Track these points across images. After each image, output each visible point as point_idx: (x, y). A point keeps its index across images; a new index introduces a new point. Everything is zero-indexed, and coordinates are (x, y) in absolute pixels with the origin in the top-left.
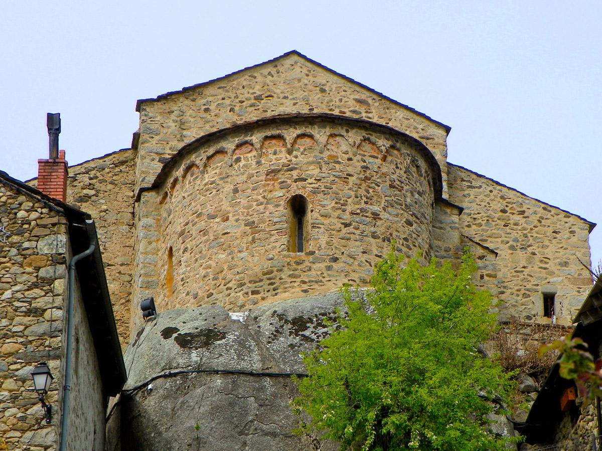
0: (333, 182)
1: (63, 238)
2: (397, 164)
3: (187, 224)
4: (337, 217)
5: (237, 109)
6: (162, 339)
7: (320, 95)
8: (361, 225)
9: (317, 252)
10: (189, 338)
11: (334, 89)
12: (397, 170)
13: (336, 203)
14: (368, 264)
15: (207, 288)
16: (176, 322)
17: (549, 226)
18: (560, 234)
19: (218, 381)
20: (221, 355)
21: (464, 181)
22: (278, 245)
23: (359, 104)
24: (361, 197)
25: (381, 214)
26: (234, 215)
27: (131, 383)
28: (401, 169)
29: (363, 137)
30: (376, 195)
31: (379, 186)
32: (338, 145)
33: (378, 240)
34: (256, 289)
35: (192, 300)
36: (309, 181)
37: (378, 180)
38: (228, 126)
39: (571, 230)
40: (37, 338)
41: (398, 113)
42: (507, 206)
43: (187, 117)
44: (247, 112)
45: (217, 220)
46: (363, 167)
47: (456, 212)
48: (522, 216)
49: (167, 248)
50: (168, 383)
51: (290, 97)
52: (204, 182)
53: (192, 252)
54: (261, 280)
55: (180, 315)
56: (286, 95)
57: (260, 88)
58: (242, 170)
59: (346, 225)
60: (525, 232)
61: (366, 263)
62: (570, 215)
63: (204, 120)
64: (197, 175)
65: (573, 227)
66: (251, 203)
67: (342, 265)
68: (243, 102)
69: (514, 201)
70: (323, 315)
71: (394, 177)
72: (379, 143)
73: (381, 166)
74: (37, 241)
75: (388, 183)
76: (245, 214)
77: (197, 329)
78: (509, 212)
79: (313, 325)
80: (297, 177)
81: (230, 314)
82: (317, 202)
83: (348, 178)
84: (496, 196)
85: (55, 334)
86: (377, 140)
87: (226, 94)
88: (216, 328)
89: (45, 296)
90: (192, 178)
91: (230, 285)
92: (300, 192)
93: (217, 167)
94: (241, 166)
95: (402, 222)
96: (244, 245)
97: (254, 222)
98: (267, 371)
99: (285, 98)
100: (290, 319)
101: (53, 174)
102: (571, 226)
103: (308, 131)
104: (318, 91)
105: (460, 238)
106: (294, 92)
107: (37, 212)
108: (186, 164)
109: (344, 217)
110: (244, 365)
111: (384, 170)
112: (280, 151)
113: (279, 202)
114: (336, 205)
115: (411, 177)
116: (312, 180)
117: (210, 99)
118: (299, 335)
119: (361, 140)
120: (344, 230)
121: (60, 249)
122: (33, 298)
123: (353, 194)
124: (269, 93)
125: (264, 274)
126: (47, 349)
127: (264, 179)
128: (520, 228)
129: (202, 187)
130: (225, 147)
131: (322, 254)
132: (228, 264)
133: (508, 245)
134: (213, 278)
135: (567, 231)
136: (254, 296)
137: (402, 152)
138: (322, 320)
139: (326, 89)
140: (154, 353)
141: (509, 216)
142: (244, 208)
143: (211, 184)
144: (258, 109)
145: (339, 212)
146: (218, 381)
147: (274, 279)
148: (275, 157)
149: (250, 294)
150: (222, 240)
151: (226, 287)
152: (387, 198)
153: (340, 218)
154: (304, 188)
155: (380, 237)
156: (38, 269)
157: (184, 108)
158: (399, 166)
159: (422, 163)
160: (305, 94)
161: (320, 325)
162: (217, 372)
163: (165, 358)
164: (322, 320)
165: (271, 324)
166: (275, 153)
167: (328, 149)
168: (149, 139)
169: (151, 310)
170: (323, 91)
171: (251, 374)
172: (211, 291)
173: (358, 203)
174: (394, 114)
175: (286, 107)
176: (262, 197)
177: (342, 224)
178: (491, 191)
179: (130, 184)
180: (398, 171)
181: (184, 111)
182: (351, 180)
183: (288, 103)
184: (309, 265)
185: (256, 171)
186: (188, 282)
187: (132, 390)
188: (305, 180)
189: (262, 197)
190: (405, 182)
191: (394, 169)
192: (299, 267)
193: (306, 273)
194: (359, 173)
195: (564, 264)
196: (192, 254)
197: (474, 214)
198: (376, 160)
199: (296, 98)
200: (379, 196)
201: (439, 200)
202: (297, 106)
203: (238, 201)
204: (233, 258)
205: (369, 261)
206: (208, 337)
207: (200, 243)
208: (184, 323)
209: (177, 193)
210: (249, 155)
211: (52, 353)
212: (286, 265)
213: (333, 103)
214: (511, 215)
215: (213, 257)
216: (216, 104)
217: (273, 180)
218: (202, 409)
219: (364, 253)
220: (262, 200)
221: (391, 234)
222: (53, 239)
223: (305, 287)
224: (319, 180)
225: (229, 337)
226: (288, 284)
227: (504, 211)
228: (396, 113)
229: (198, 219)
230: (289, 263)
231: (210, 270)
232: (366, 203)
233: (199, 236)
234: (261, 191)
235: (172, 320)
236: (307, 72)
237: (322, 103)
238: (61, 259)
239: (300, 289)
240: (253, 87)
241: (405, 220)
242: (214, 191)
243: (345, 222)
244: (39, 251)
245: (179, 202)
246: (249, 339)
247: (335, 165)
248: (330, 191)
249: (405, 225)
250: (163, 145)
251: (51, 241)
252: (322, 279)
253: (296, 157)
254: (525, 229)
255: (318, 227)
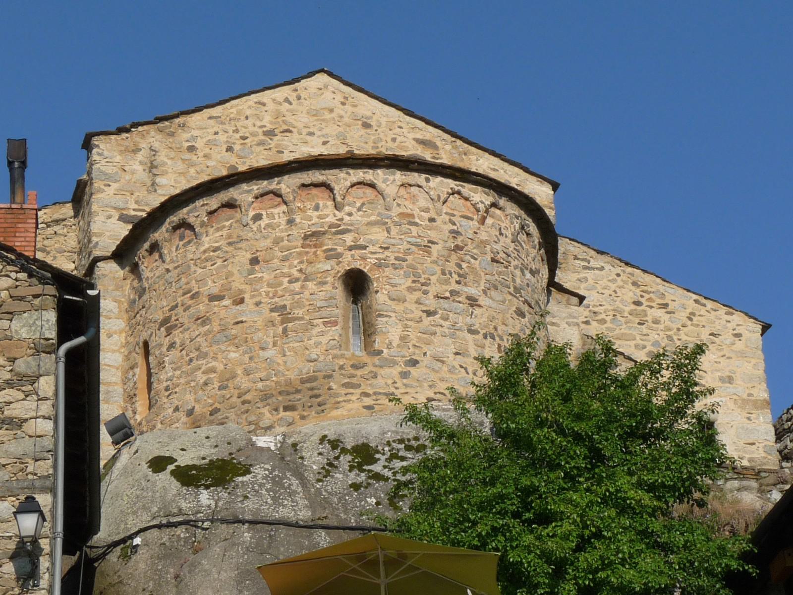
0: (407, 252)
1: (51, 316)
2: (500, 229)
3: (172, 309)
4: (416, 302)
5: (237, 147)
6: (151, 473)
7: (363, 131)
8: (451, 315)
9: (385, 351)
10: (194, 472)
11: (384, 124)
12: (500, 237)
13: (414, 282)
14: (463, 370)
15: (210, 401)
16: (171, 448)
17: (704, 326)
18: (720, 337)
19: (246, 534)
20: (246, 497)
21: (578, 259)
22: (324, 340)
23: (422, 146)
24: (450, 274)
25: (480, 299)
26: (253, 297)
27: (104, 535)
28: (506, 237)
29: (451, 189)
30: (472, 272)
31: (476, 259)
32: (414, 199)
33: (477, 337)
34: (290, 403)
35: (184, 419)
36: (371, 248)
37: (475, 251)
38: (224, 173)
39: (735, 332)
40: (15, 460)
41: (481, 161)
42: (642, 296)
43: (162, 157)
44: (252, 152)
45: (226, 302)
46: (452, 232)
47: (575, 300)
48: (664, 310)
49: (137, 344)
50: (165, 536)
51: (318, 133)
52: (202, 249)
53: (183, 349)
54: (298, 391)
55: (175, 439)
56: (311, 130)
57: (272, 119)
58: (263, 231)
59: (429, 313)
60: (669, 333)
61: (460, 369)
62: (734, 312)
63: (187, 162)
64: (189, 239)
65: (738, 328)
66: (281, 279)
67: (424, 370)
68: (247, 138)
69: (652, 290)
70: (401, 441)
71: (497, 247)
72: (474, 199)
73: (478, 231)
74: (11, 320)
75: (489, 257)
76: (271, 295)
77: (204, 458)
78: (645, 305)
79: (386, 457)
80: (353, 244)
81: (254, 438)
82: (385, 279)
83: (430, 247)
84: (625, 282)
85: (41, 456)
86: (472, 194)
87: (220, 126)
88: (233, 458)
89: (23, 400)
90: (181, 243)
91: (248, 397)
92: (358, 265)
93: (224, 227)
94: (263, 226)
95: (511, 311)
96: (270, 340)
97: (284, 307)
98: (320, 522)
99: (311, 134)
100: (349, 447)
101: (20, 225)
102: (735, 327)
103: (368, 179)
104: (360, 126)
105: (582, 338)
106: (323, 126)
107: (9, 277)
108: (173, 222)
109: (427, 302)
110: (284, 512)
111: (483, 236)
112: (326, 206)
113: (326, 278)
114: (414, 285)
115: (519, 248)
116: (375, 248)
117: (195, 133)
118: (365, 470)
119: (448, 193)
120: (427, 321)
121: (47, 332)
122: (5, 402)
123: (438, 269)
124: (285, 127)
125: (303, 382)
126: (30, 477)
127: (300, 245)
128: (661, 327)
129: (198, 255)
130: (237, 198)
131: (394, 354)
132: (244, 366)
133: (644, 350)
134: (219, 387)
135: (730, 334)
136: (288, 413)
137: (507, 213)
138: (398, 450)
139: (372, 123)
140: (138, 492)
141: (645, 311)
142: (269, 285)
143: (214, 251)
144: (270, 149)
145: (417, 295)
146: (246, 534)
147: (319, 389)
148: (316, 213)
149: (281, 409)
150: (234, 332)
151: (242, 399)
152: (488, 277)
153: (420, 304)
154: (363, 258)
155: (479, 333)
156: (13, 360)
157: (156, 145)
158: (503, 231)
159: (533, 228)
160: (341, 129)
161: (394, 456)
162: (243, 522)
163: (158, 500)
164: (398, 450)
165: (320, 454)
166: (317, 208)
167: (399, 205)
168: (102, 187)
169: (127, 429)
170: (367, 126)
171: (296, 525)
172: (217, 405)
173: (447, 282)
174: (475, 162)
175: (312, 147)
176: (297, 270)
177: (423, 311)
178: (618, 275)
179: (69, 252)
180: (502, 239)
181: (157, 150)
182: (435, 249)
183: (316, 141)
184: (374, 369)
185: (287, 234)
186: (176, 393)
187: (104, 547)
188: (365, 247)
189: (297, 270)
190: (512, 255)
191: (496, 236)
192: (359, 373)
193: (369, 382)
194: (446, 239)
195: (727, 379)
196: (184, 352)
197: (594, 306)
198: (471, 223)
199: (327, 134)
200: (476, 274)
201: (553, 285)
202: (328, 145)
203: (259, 275)
204: (251, 358)
205: (464, 366)
206: (220, 472)
207: (197, 336)
208: (183, 450)
209: (155, 264)
210: (276, 211)
211: (38, 484)
212: (337, 368)
213: (383, 143)
214: (648, 309)
215: (219, 356)
216: (205, 140)
217: (316, 246)
218: (224, 575)
219: (457, 354)
220: (297, 274)
221: (496, 328)
222: (35, 317)
223: (368, 401)
224: (387, 248)
225: (256, 471)
226: (341, 396)
227: (638, 303)
228: (477, 160)
229: (193, 301)
230: (343, 365)
231: (215, 375)
232: (458, 282)
233: (195, 326)
234: (296, 262)
235: (163, 446)
236: (342, 100)
237: (366, 143)
238: (47, 346)
239: (360, 404)
240: (261, 118)
241: (514, 309)
242: (219, 262)
243: (428, 309)
244: (14, 334)
245: (158, 277)
246: (288, 474)
247: (410, 227)
248: (404, 264)
249: (515, 316)
250: (124, 197)
251: (33, 320)
252: (394, 391)
253: (350, 214)
254: (670, 329)
255: (387, 316)
